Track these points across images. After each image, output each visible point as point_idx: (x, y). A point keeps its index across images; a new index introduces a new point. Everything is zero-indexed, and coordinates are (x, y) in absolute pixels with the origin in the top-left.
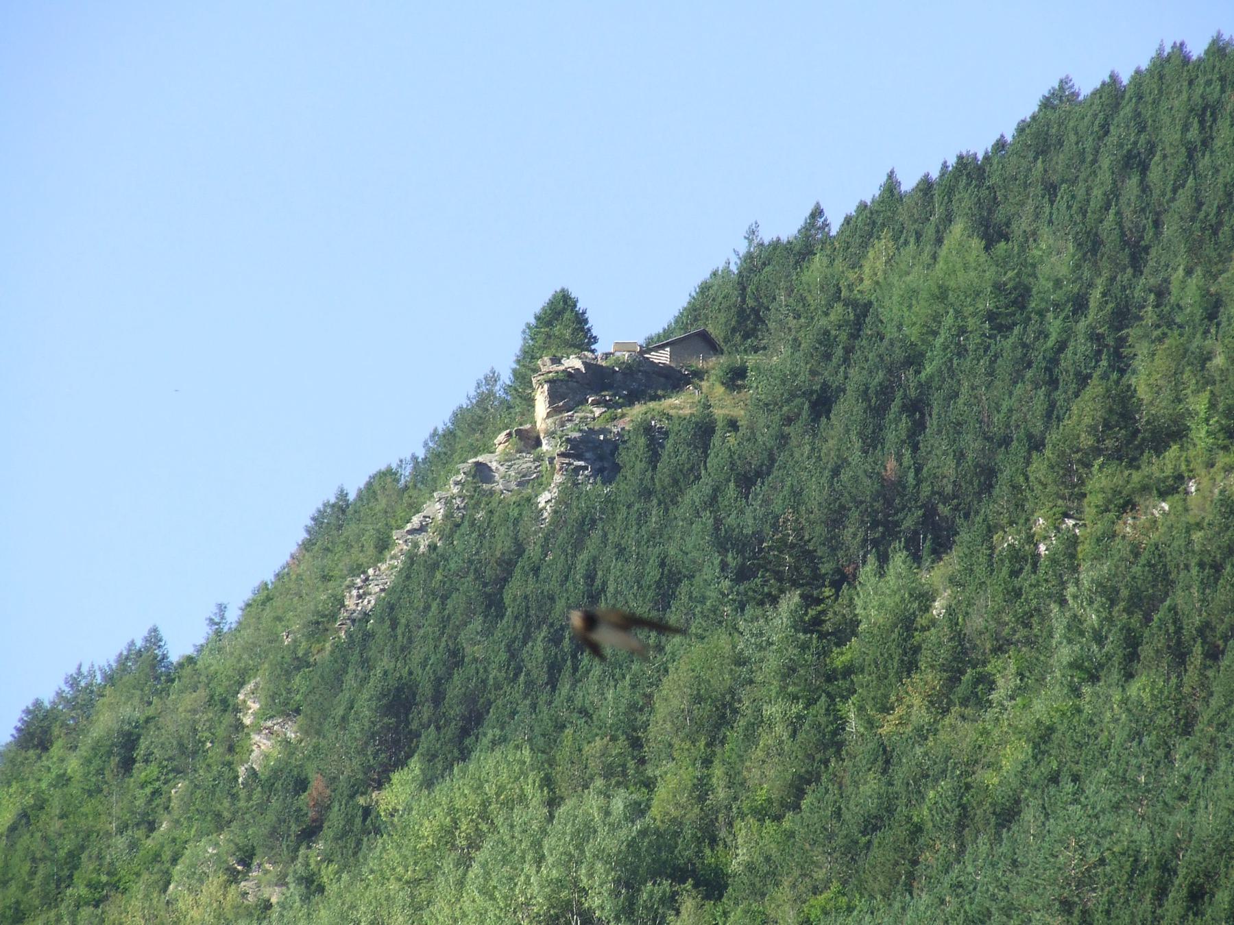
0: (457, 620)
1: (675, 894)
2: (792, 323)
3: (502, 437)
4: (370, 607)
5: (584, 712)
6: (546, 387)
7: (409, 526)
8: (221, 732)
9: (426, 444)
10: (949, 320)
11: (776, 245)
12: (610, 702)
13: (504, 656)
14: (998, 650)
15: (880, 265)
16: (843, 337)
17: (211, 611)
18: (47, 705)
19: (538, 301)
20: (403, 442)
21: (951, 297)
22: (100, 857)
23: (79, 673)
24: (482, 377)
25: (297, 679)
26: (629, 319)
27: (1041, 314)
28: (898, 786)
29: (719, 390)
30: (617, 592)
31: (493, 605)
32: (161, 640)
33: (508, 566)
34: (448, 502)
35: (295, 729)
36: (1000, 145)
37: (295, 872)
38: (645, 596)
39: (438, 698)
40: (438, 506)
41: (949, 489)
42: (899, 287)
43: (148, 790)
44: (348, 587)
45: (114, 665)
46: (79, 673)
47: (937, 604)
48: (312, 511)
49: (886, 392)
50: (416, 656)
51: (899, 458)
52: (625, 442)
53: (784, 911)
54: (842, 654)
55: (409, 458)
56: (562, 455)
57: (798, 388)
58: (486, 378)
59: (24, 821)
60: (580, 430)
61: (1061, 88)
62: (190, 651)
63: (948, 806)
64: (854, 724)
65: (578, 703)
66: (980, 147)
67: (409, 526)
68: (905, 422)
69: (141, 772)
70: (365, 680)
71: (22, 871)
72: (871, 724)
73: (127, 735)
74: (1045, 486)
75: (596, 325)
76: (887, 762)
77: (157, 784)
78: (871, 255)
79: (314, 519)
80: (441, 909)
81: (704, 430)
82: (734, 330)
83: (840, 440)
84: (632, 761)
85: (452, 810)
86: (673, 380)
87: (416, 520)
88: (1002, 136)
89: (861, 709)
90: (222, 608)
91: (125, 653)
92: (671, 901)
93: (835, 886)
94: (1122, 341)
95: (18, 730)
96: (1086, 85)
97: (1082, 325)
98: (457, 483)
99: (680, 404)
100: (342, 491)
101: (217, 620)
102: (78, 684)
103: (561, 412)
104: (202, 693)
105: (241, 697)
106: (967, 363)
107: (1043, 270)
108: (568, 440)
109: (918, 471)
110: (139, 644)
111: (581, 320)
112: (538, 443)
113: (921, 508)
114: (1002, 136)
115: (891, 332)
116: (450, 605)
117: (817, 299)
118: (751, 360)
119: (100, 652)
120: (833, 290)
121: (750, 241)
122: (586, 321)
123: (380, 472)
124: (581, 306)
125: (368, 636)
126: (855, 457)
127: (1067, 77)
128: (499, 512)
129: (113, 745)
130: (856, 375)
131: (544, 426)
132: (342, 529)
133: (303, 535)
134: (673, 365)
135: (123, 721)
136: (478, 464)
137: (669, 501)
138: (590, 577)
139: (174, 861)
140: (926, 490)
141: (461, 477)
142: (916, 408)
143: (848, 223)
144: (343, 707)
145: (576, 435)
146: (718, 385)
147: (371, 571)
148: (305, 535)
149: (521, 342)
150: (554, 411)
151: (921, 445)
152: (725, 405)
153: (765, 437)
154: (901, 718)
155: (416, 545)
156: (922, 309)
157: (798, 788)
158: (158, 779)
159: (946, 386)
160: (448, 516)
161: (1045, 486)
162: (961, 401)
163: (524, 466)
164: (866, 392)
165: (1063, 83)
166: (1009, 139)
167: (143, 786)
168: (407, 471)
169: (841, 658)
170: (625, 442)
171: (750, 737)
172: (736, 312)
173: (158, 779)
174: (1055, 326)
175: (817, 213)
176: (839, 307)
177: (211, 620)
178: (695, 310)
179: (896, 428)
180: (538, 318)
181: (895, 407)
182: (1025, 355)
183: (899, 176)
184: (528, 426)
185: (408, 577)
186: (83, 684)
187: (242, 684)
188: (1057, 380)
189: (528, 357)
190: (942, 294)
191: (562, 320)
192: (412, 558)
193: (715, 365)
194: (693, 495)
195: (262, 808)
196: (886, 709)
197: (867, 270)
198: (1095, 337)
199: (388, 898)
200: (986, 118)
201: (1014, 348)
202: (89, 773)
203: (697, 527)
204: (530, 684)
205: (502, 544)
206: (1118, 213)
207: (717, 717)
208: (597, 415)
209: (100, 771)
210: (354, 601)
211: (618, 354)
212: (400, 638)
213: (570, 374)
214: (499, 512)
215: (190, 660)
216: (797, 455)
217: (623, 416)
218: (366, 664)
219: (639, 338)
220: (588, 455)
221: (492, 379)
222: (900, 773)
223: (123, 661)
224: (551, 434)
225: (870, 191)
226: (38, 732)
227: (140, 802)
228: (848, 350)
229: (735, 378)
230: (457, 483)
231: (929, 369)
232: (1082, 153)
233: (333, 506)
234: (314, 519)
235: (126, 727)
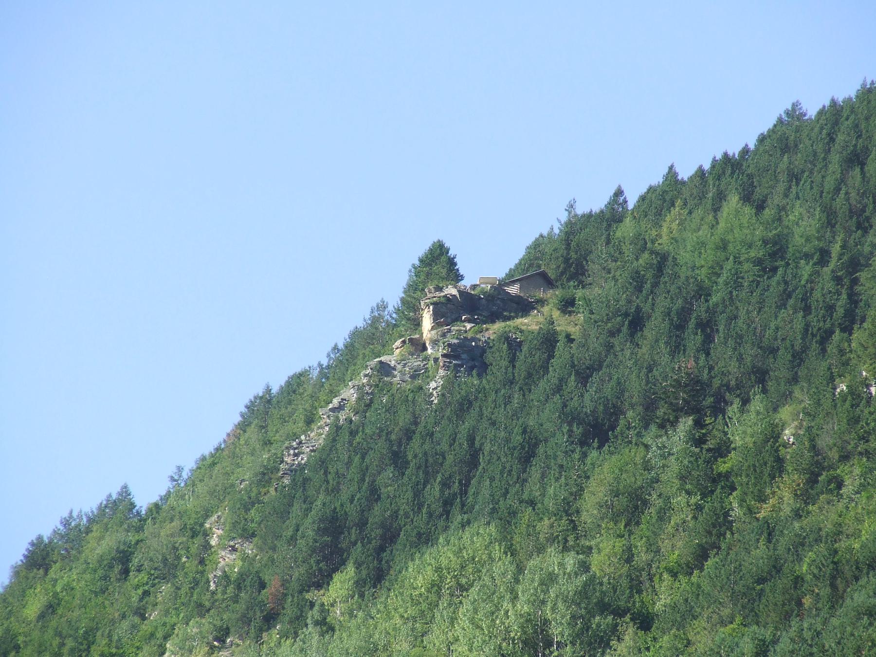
0: (373, 470)
1: (617, 625)
2: (612, 265)
3: (398, 343)
4: (303, 462)
5: (532, 503)
6: (431, 307)
7: (331, 406)
8: (194, 549)
9: (328, 355)
10: (729, 265)
11: (589, 216)
12: (554, 493)
13: (410, 495)
14: (845, 457)
15: (674, 226)
16: (649, 275)
17: (171, 471)
18: (46, 540)
19: (422, 248)
20: (313, 353)
21: (731, 247)
22: (110, 636)
23: (71, 516)
24: (375, 305)
25: (253, 512)
26: (485, 263)
27: (796, 260)
28: (781, 550)
29: (556, 314)
30: (491, 452)
31: (398, 460)
32: (129, 495)
33: (409, 434)
34: (360, 388)
35: (251, 547)
36: (745, 151)
37: (313, 617)
38: (512, 455)
39: (362, 524)
40: (352, 391)
41: (733, 383)
42: (688, 241)
43: (140, 592)
44: (287, 448)
45: (95, 512)
46: (71, 516)
47: (787, 432)
48: (246, 401)
49: (685, 313)
50: (345, 495)
51: (697, 359)
52: (491, 347)
53: (702, 636)
54: (725, 463)
55: (316, 365)
56: (444, 356)
57: (619, 310)
58: (378, 306)
59: (50, 611)
60: (457, 338)
61: (794, 110)
62: (155, 499)
63: (824, 562)
64: (737, 511)
65: (525, 496)
66: (734, 150)
67: (331, 406)
68: (699, 338)
69: (135, 578)
70: (309, 509)
71: (54, 645)
72: (750, 511)
73: (111, 559)
74: (866, 348)
75: (462, 267)
76: (770, 534)
77: (146, 588)
78: (668, 218)
79: (247, 407)
80: (436, 638)
81: (549, 340)
82: (562, 273)
83: (652, 347)
84: (572, 535)
85: (438, 569)
86: (523, 307)
87: (336, 401)
88: (747, 145)
89: (742, 501)
90: (180, 469)
91: (105, 502)
92: (614, 632)
93: (738, 619)
94: (855, 281)
95: (25, 556)
96: (811, 109)
97: (827, 270)
98: (366, 376)
99: (530, 323)
100: (268, 387)
101: (176, 478)
102: (70, 525)
103: (442, 326)
104: (176, 523)
105: (207, 525)
106: (743, 294)
107: (797, 231)
108: (449, 345)
109: (711, 368)
110: (114, 497)
111: (452, 263)
112: (424, 348)
113: (713, 396)
114: (747, 145)
115: (684, 272)
116: (367, 460)
117: (628, 250)
118: (579, 293)
119: (87, 501)
120: (641, 242)
121: (570, 213)
122: (455, 264)
123: (295, 374)
124: (451, 253)
125: (306, 480)
126: (665, 359)
127: (798, 102)
128: (398, 396)
129: (113, 558)
130: (662, 303)
131: (429, 336)
132: (265, 413)
133: (238, 419)
134: (522, 295)
135: (119, 542)
136: (381, 362)
137: (525, 390)
138: (471, 440)
139: (166, 638)
140: (716, 383)
141: (369, 371)
142: (707, 327)
143: (643, 200)
144: (291, 529)
145: (456, 341)
146: (555, 310)
147: (303, 437)
148: (239, 419)
149: (408, 278)
150: (437, 325)
151: (712, 351)
152: (564, 325)
153: (596, 345)
154: (774, 506)
155: (337, 418)
156: (709, 256)
157: (702, 555)
158: (147, 584)
159: (728, 310)
160: (359, 399)
161: (866, 348)
162: (740, 322)
163: (416, 364)
164: (669, 314)
165: (795, 105)
166: (752, 146)
167: (137, 587)
168: (315, 374)
169: (723, 467)
170: (491, 347)
171: (663, 516)
172: (565, 259)
173: (147, 584)
174: (806, 269)
175: (619, 193)
176: (646, 255)
177: (172, 477)
178: (531, 260)
179: (693, 340)
180: (421, 261)
181: (692, 324)
182: (786, 290)
183: (678, 169)
184: (417, 336)
185: (334, 440)
186: (73, 524)
187: (207, 516)
188: (810, 307)
189: (415, 289)
190: (723, 246)
191: (438, 262)
192: (337, 428)
193: (553, 295)
194: (543, 385)
195: (236, 599)
196: (762, 498)
197: (665, 230)
198: (838, 280)
199: (394, 629)
200: (740, 131)
201: (778, 283)
202: (94, 579)
203: (549, 406)
204: (430, 515)
205: (403, 419)
206: (847, 193)
207: (631, 507)
208: (468, 328)
209: (105, 578)
210: (291, 458)
211: (483, 286)
212: (331, 482)
213: (448, 300)
214: (398, 396)
215: (157, 506)
216: (620, 358)
217: (487, 329)
218: (308, 501)
219: (500, 273)
220: (464, 356)
221: (382, 306)
222: (783, 542)
223: (102, 509)
224: (435, 343)
225: (657, 178)
226: (39, 559)
227: (135, 599)
228: (655, 285)
229: (567, 306)
230: (366, 376)
231: (714, 299)
232: (815, 154)
233: (261, 398)
234: (247, 407)
235: (122, 547)
